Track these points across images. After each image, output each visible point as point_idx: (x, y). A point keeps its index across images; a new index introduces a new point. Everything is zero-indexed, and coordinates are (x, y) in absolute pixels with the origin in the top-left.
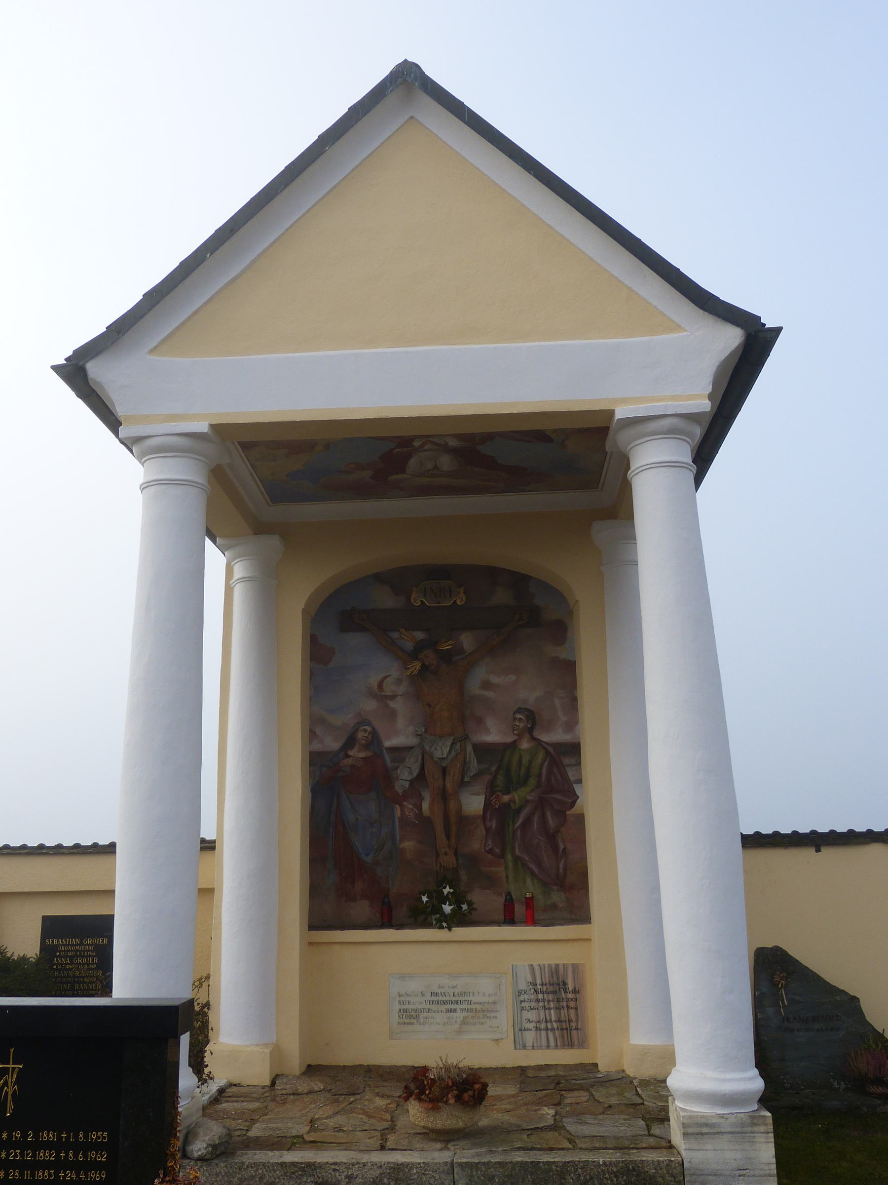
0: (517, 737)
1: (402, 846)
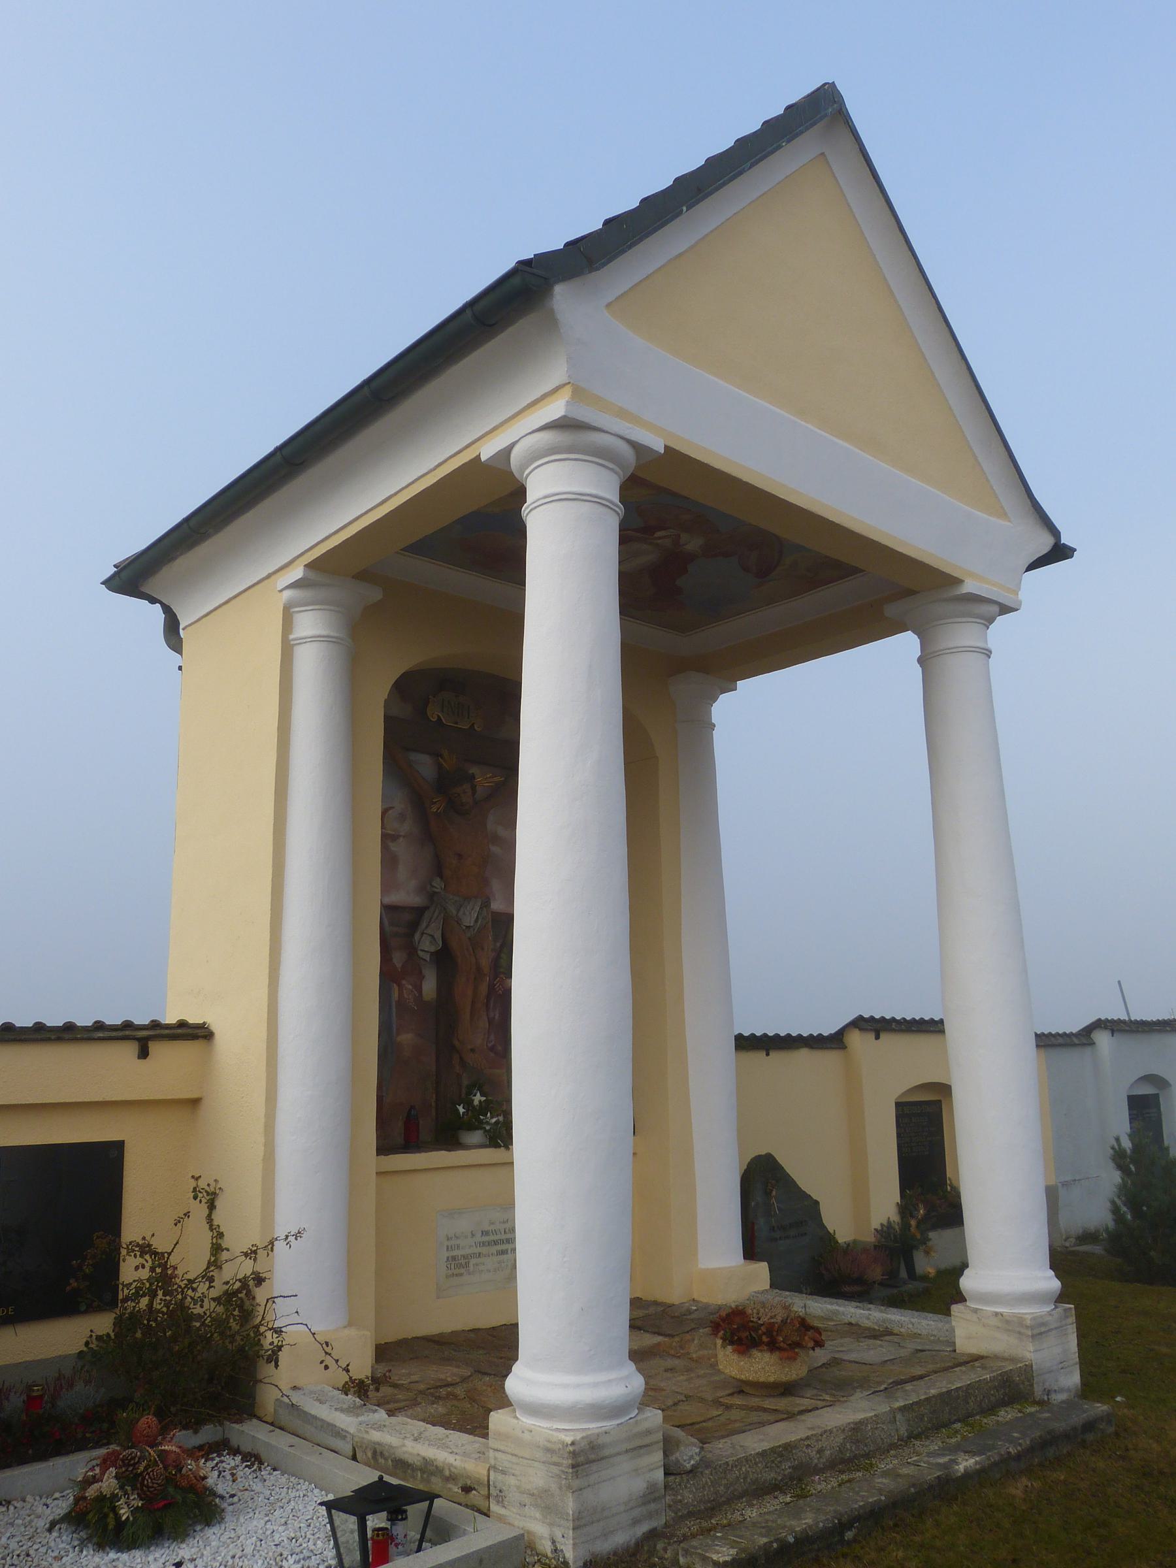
1: (399, 1039)
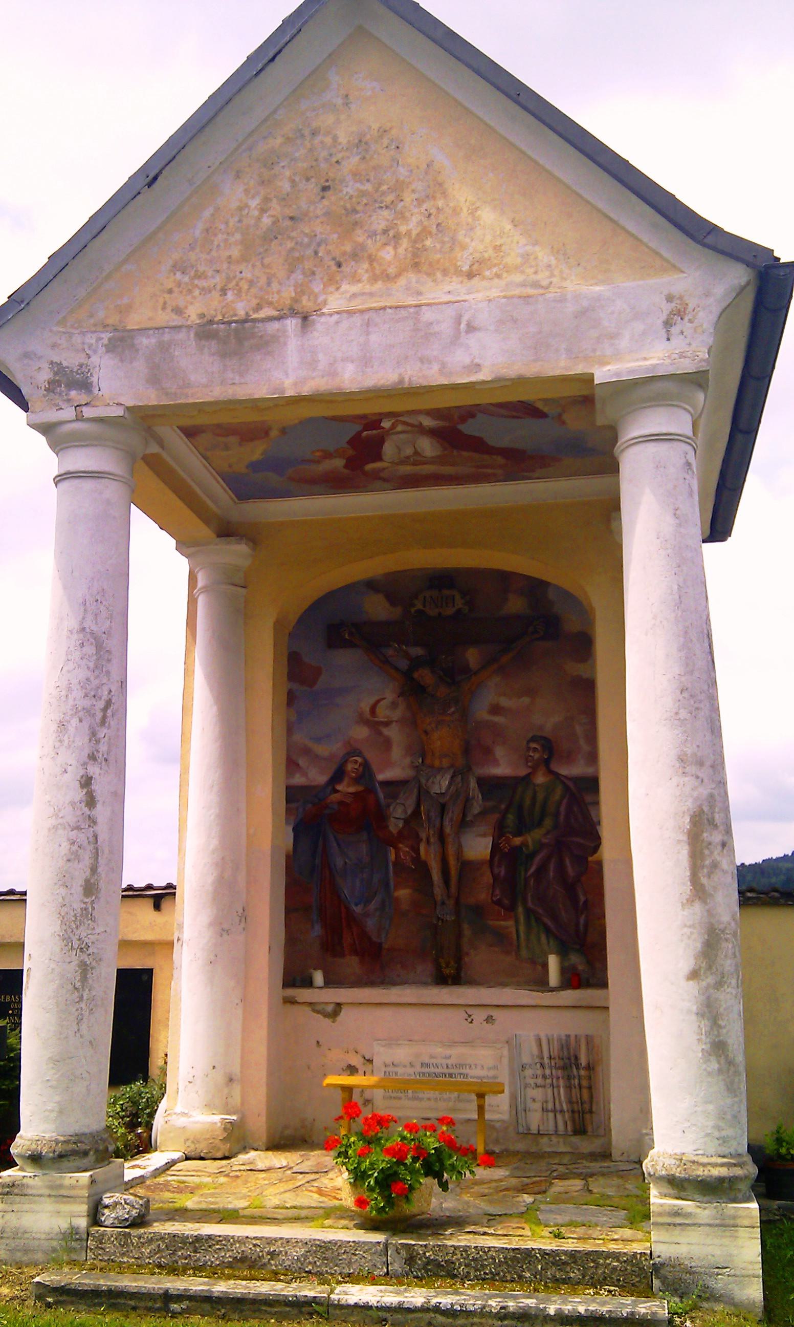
0: (530, 770)
1: (396, 894)
